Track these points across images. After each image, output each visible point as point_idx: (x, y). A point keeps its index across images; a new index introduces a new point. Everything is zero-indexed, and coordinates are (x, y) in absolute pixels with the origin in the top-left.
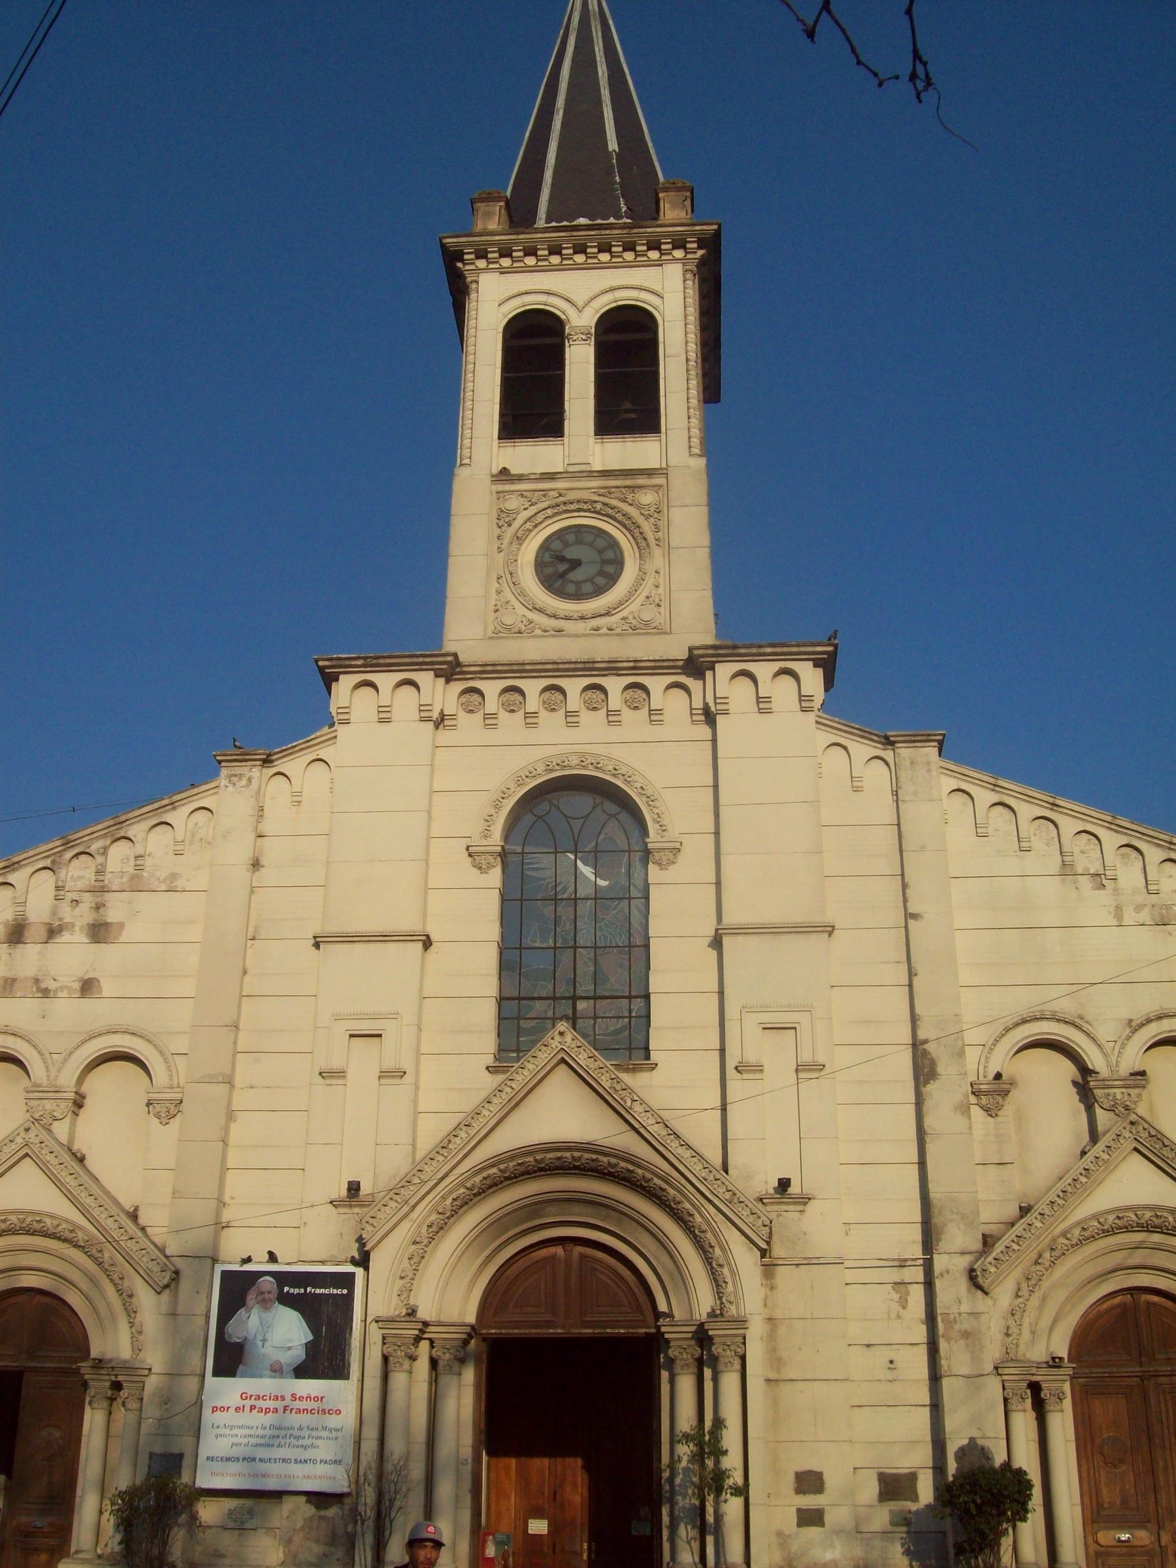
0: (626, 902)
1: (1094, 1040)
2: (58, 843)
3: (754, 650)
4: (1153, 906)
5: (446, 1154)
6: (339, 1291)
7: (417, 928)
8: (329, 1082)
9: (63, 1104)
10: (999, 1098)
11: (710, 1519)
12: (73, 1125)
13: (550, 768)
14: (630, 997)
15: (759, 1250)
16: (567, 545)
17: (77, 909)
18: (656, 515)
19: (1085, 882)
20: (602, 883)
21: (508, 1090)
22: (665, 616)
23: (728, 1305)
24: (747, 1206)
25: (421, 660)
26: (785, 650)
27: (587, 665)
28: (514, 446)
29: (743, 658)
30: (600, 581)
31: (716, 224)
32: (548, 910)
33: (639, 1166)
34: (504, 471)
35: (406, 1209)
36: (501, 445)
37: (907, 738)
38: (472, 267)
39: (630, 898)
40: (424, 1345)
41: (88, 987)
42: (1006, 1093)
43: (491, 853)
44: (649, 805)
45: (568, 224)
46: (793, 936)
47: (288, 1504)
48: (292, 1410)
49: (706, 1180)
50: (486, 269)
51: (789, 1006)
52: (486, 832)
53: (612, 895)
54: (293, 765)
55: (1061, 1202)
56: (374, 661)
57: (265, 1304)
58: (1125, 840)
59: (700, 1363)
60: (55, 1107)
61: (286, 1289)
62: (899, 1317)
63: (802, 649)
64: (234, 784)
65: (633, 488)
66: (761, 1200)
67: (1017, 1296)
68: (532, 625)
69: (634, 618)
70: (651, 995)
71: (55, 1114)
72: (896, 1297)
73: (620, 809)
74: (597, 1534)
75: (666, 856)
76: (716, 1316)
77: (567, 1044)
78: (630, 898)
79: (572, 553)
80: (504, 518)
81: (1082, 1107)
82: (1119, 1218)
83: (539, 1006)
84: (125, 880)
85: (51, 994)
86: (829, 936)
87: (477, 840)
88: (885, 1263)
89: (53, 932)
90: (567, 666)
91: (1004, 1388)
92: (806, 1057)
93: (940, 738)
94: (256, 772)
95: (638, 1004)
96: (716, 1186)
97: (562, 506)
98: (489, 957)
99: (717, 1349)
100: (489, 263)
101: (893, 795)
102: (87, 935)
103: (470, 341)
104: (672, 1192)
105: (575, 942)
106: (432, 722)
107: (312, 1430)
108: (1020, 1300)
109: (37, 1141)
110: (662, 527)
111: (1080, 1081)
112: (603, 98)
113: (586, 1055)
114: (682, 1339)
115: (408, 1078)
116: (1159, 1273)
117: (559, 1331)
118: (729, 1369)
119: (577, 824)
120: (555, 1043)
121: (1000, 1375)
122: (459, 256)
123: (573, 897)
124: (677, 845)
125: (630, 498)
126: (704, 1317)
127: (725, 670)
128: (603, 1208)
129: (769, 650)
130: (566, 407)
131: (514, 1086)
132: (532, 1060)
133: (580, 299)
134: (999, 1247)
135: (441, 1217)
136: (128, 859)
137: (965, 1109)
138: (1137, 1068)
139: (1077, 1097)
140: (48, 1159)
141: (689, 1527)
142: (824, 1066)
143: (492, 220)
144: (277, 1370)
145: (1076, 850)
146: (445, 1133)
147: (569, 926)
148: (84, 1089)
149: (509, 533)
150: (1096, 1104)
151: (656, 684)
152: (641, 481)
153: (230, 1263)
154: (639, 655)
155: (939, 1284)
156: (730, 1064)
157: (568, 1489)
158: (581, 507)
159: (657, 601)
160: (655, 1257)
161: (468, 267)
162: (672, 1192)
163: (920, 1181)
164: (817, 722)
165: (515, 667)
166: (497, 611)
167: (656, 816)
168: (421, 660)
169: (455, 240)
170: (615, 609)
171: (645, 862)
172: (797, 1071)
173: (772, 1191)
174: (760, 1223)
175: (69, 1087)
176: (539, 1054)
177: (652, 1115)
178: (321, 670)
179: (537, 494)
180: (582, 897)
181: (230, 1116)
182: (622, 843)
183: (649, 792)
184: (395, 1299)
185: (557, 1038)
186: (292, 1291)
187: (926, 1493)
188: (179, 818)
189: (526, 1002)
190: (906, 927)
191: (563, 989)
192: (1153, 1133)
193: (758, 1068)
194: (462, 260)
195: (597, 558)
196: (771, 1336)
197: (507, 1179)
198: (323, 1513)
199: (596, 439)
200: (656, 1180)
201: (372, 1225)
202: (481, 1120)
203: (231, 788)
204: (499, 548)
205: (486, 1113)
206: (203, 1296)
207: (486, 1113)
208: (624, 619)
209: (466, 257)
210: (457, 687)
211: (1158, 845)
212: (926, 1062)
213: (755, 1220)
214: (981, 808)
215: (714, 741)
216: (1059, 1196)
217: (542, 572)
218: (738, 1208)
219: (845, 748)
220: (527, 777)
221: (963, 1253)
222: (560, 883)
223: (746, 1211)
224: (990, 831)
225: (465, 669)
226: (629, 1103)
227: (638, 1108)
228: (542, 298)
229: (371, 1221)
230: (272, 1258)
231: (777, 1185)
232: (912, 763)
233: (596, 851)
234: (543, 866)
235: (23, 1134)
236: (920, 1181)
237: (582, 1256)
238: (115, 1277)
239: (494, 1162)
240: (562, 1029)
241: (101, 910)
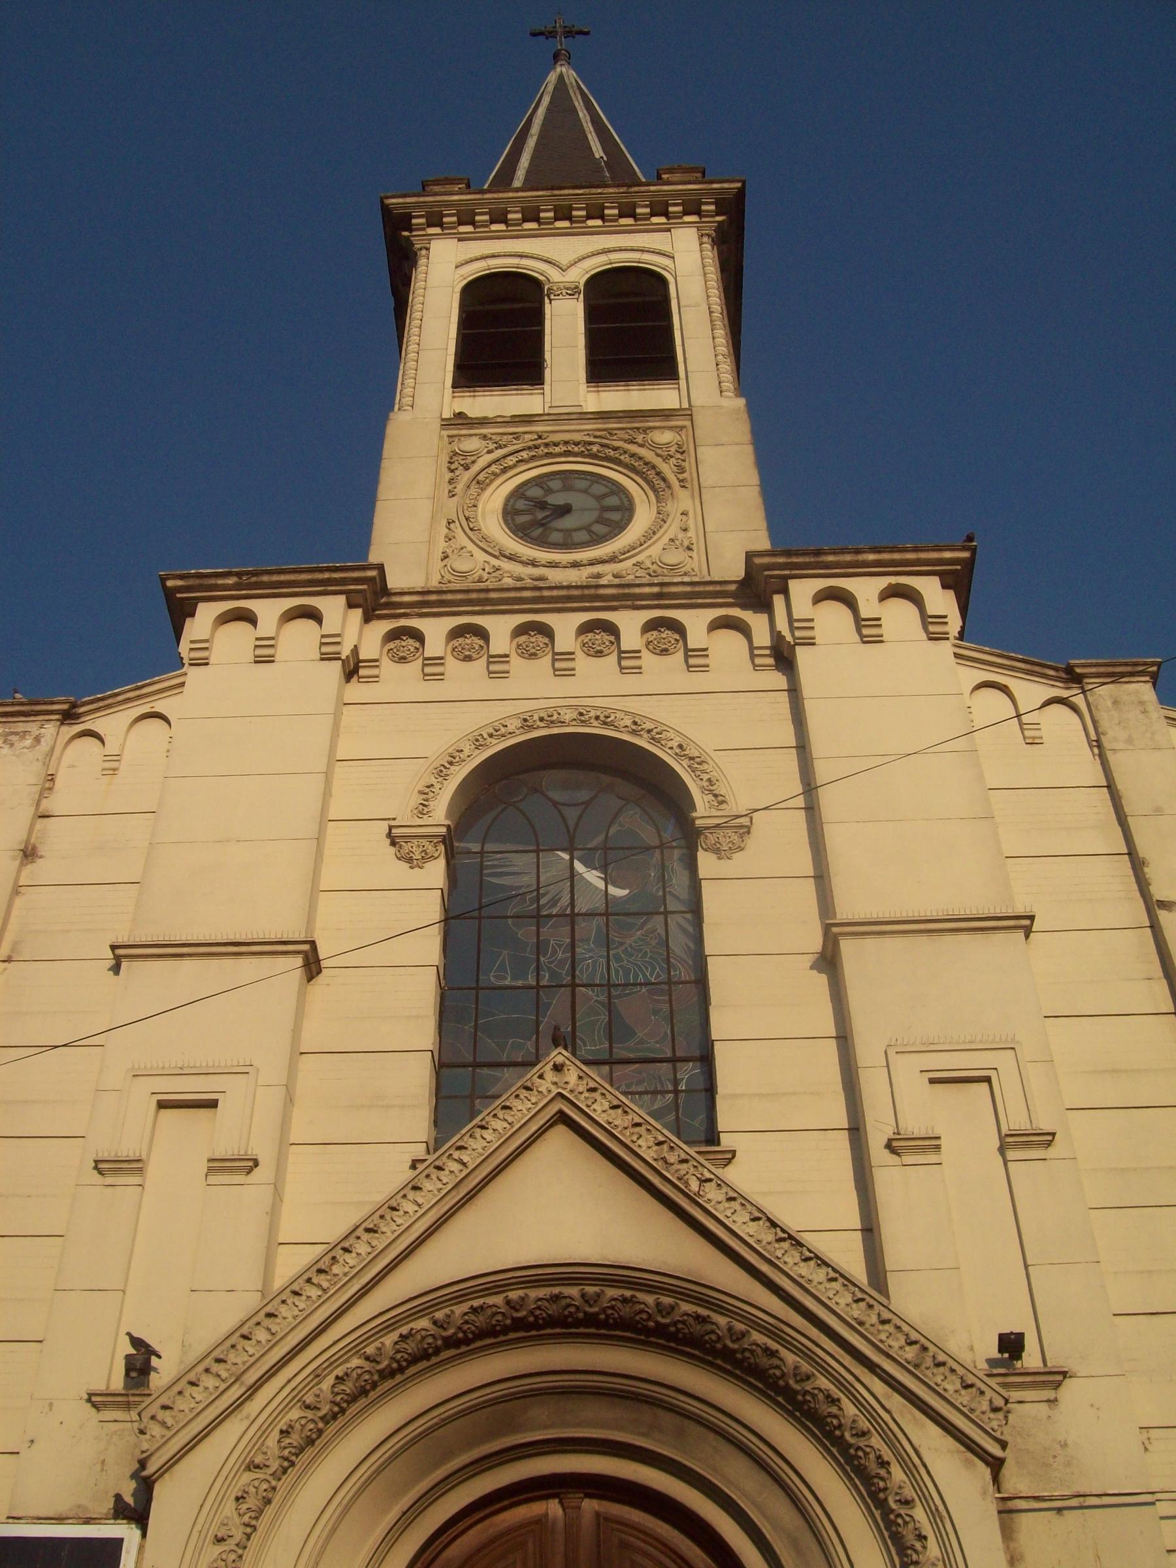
0: (661, 918)
3: (848, 558)
5: (325, 1285)
7: (293, 930)
8: (109, 1180)
14: (674, 1060)
15: (987, 1463)
16: (550, 491)
18: (678, 456)
20: (614, 891)
21: (455, 1166)
22: (700, 561)
24: (953, 1371)
25: (326, 575)
26: (897, 556)
28: (474, 396)
29: (829, 570)
31: (739, 181)
32: (526, 933)
35: (235, 1392)
36: (456, 394)
37: (1102, 670)
39: (666, 913)
46: (964, 937)
49: (861, 1323)
52: (421, 807)
53: (634, 908)
63: (923, 555)
64: (12, 745)
68: (500, 572)
69: (653, 563)
70: (717, 1045)
75: (726, 838)
77: (569, 1087)
78: (666, 913)
80: (457, 461)
86: (1027, 937)
87: (405, 816)
92: (1016, 1120)
93: (1154, 669)
95: (688, 1072)
96: (883, 1336)
97: (542, 448)
101: (1091, 747)
103: (411, 347)
104: (790, 1358)
105: (573, 977)
106: (340, 662)
110: (687, 468)
113: (606, 1105)
120: (547, 1084)
122: (404, 221)
123: (568, 912)
125: (640, 439)
127: (802, 590)
128: (645, 1407)
129: (871, 557)
130: (547, 356)
131: (466, 1159)
132: (501, 1114)
133: (564, 261)
135: (310, 1414)
142: (1053, 1134)
149: (466, 476)
151: (696, 621)
156: (876, 1140)
158: (570, 448)
159: (686, 543)
162: (790, 1358)
164: (956, 655)
165: (474, 596)
167: (706, 784)
168: (326, 575)
169: (401, 200)
170: (624, 554)
172: (1002, 1150)
174: (985, 1406)
176: (516, 1104)
177: (743, 1205)
178: (169, 593)
180: (584, 911)
182: (648, 835)
185: (550, 1076)
193: (931, 1144)
197: (450, 1343)
199: (588, 387)
200: (756, 1336)
201: (163, 1424)
202: (399, 1221)
204: (450, 491)
205: (409, 1207)
207: (409, 1207)
209: (414, 221)
210: (382, 627)
213: (973, 1399)
215: (794, 692)
217: (513, 520)
218: (936, 1377)
219: (1004, 689)
220: (491, 736)
222: (544, 895)
223: (953, 1382)
226: (694, 1185)
229: (162, 1415)
233: (606, 848)
234: (515, 869)
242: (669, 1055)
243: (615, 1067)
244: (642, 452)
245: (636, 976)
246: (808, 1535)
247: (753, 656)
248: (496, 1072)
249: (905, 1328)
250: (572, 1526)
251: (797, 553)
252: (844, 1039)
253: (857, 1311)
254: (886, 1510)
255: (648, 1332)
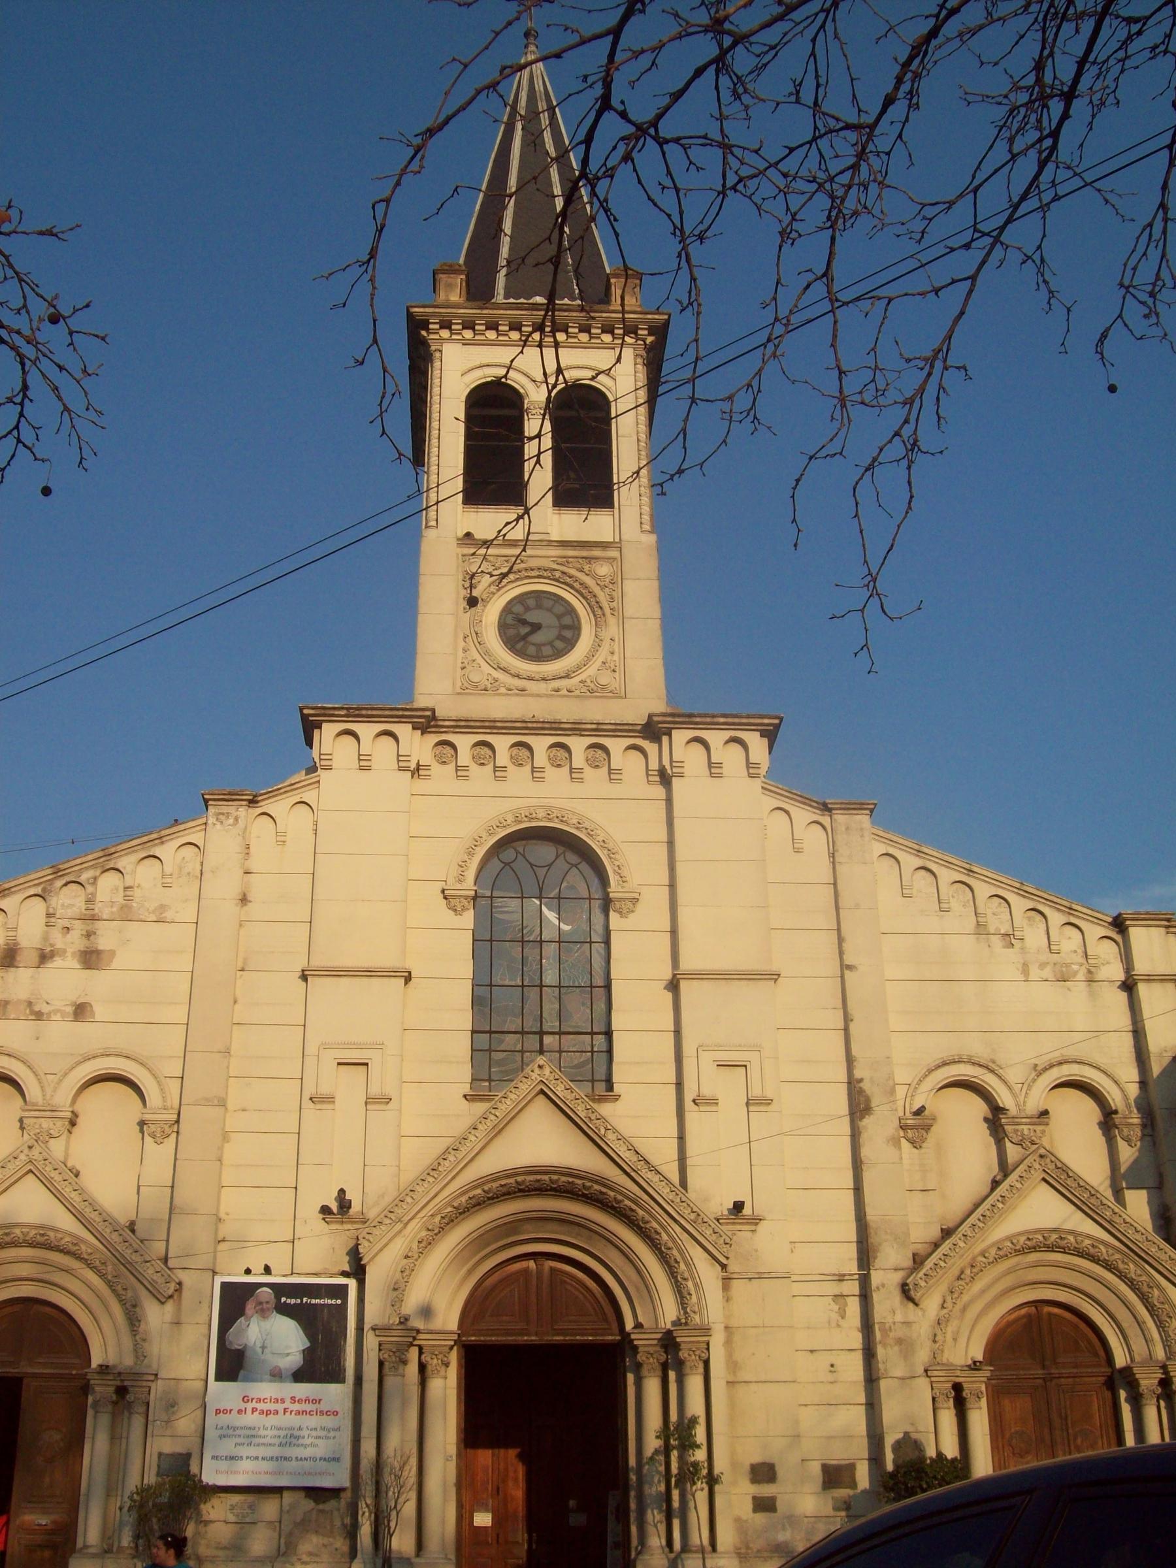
1: (1005, 1082)
2: (49, 871)
3: (708, 720)
4: (1055, 964)
6: (333, 1302)
8: (318, 1106)
9: (59, 1123)
10: (923, 1131)
11: (676, 1504)
12: (68, 1142)
13: (519, 819)
14: (592, 1033)
16: (527, 609)
17: (69, 936)
18: (611, 586)
19: (996, 941)
21: (493, 1117)
23: (692, 1315)
25: (401, 713)
26: (736, 720)
27: (553, 725)
29: (696, 725)
30: (559, 644)
33: (611, 1189)
34: (468, 535)
37: (843, 806)
38: (436, 337)
39: (591, 942)
40: (414, 1352)
41: (81, 1011)
42: (927, 1128)
43: (466, 897)
44: (610, 858)
45: (525, 301)
48: (291, 1412)
50: (450, 340)
51: (740, 1046)
54: (278, 806)
55: (981, 1225)
56: (357, 712)
57: (263, 1313)
58: (1031, 905)
59: (665, 1368)
60: (51, 1126)
61: (283, 1299)
62: (838, 1326)
63: (752, 721)
65: (589, 559)
66: (718, 1220)
67: (943, 1307)
71: (51, 1132)
72: (836, 1308)
73: (580, 861)
74: (533, 1521)
76: (681, 1325)
78: (591, 942)
79: (532, 617)
81: (992, 1140)
82: (1029, 1239)
83: (510, 1038)
84: (114, 909)
85: (45, 1017)
87: (453, 886)
88: (825, 1277)
89: (44, 957)
90: (535, 725)
91: (932, 1389)
92: (756, 1092)
93: (872, 807)
94: (243, 812)
98: (463, 994)
99: (683, 1354)
100: (452, 334)
102: (80, 962)
104: (641, 1212)
107: (311, 1430)
108: (945, 1311)
109: (41, 1158)
111: (990, 1116)
112: (553, 179)
114: (651, 1345)
116: (1052, 1286)
117: (533, 1338)
118: (694, 1372)
119: (541, 872)
121: (930, 1377)
122: (425, 325)
124: (636, 896)
125: (587, 568)
126: (669, 1326)
127: (680, 736)
129: (722, 720)
131: (497, 1114)
134: (929, 1263)
135: (429, 1233)
136: (117, 889)
137: (896, 1142)
138: (1042, 1108)
139: (988, 1132)
140: (52, 1175)
141: (656, 1512)
143: (453, 292)
144: (277, 1375)
145: (989, 912)
146: (435, 1156)
147: (536, 967)
148: (78, 1107)
150: (1006, 1139)
151: (616, 746)
152: (597, 553)
153: (229, 1275)
154: (598, 717)
155: (876, 1297)
156: (688, 1097)
157: (510, 1484)
159: (613, 667)
160: (622, 1271)
161: (432, 336)
162: (641, 1212)
163: (856, 1204)
164: (762, 787)
165: (487, 724)
166: (463, 668)
167: (617, 869)
168: (401, 713)
169: (421, 310)
171: (606, 911)
173: (726, 1212)
174: (722, 1241)
175: (64, 1106)
179: (500, 559)
181: (225, 1136)
183: (610, 846)
184: (389, 1310)
185: (537, 1071)
186: (289, 1301)
187: (863, 1477)
188: (166, 851)
189: (496, 1035)
190: (842, 977)
191: (531, 1024)
192: (1059, 1165)
193: (713, 1102)
194: (427, 329)
195: (555, 622)
196: (728, 1342)
198: (321, 1507)
200: (627, 1202)
201: (369, 1241)
203: (218, 826)
206: (205, 1305)
208: (582, 682)
209: (431, 326)
211: (1059, 910)
212: (862, 1099)
214: (907, 870)
215: (669, 801)
216: (979, 1220)
218: (703, 1228)
219: (787, 812)
221: (896, 1269)
224: (914, 891)
225: (441, 723)
226: (603, 1131)
227: (611, 1136)
229: (367, 1237)
230: (267, 1270)
231: (732, 1206)
232: (847, 829)
235: (26, 1151)
236: (855, 1204)
237: (552, 1269)
238: (119, 1288)
239: (480, 1183)
240: (541, 1062)
241: (92, 938)
242: (590, 1030)
243: (562, 1036)
244: (588, 580)
245: (574, 982)
246: (643, 1286)
247: (648, 775)
248: (502, 1036)
249: (692, 1205)
250: (539, 1272)
251: (679, 716)
252: (677, 1032)
253: (671, 1196)
254: (677, 1281)
255: (578, 1195)
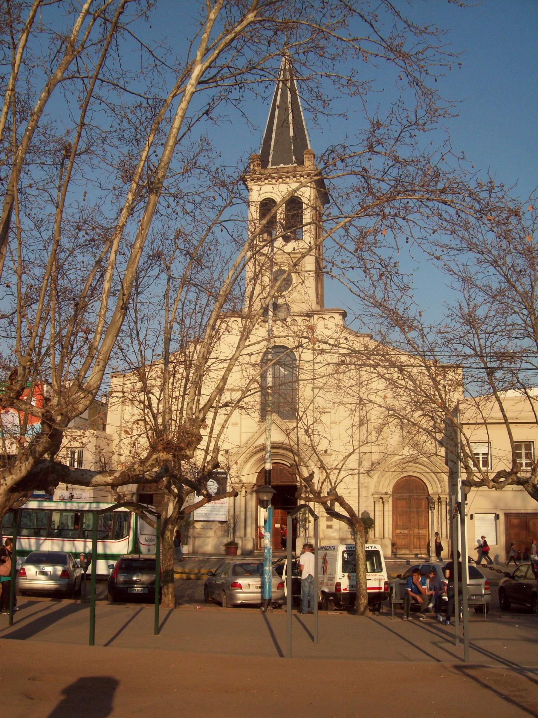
20: (286, 373)
47: (214, 523)
115: (239, 425)
127: (316, 317)
228: (270, 194)
